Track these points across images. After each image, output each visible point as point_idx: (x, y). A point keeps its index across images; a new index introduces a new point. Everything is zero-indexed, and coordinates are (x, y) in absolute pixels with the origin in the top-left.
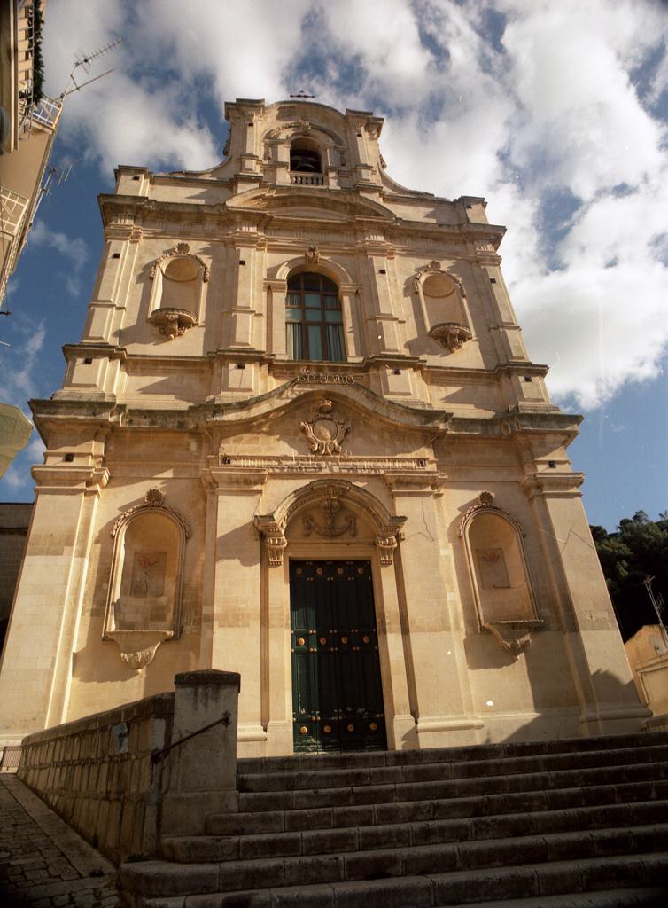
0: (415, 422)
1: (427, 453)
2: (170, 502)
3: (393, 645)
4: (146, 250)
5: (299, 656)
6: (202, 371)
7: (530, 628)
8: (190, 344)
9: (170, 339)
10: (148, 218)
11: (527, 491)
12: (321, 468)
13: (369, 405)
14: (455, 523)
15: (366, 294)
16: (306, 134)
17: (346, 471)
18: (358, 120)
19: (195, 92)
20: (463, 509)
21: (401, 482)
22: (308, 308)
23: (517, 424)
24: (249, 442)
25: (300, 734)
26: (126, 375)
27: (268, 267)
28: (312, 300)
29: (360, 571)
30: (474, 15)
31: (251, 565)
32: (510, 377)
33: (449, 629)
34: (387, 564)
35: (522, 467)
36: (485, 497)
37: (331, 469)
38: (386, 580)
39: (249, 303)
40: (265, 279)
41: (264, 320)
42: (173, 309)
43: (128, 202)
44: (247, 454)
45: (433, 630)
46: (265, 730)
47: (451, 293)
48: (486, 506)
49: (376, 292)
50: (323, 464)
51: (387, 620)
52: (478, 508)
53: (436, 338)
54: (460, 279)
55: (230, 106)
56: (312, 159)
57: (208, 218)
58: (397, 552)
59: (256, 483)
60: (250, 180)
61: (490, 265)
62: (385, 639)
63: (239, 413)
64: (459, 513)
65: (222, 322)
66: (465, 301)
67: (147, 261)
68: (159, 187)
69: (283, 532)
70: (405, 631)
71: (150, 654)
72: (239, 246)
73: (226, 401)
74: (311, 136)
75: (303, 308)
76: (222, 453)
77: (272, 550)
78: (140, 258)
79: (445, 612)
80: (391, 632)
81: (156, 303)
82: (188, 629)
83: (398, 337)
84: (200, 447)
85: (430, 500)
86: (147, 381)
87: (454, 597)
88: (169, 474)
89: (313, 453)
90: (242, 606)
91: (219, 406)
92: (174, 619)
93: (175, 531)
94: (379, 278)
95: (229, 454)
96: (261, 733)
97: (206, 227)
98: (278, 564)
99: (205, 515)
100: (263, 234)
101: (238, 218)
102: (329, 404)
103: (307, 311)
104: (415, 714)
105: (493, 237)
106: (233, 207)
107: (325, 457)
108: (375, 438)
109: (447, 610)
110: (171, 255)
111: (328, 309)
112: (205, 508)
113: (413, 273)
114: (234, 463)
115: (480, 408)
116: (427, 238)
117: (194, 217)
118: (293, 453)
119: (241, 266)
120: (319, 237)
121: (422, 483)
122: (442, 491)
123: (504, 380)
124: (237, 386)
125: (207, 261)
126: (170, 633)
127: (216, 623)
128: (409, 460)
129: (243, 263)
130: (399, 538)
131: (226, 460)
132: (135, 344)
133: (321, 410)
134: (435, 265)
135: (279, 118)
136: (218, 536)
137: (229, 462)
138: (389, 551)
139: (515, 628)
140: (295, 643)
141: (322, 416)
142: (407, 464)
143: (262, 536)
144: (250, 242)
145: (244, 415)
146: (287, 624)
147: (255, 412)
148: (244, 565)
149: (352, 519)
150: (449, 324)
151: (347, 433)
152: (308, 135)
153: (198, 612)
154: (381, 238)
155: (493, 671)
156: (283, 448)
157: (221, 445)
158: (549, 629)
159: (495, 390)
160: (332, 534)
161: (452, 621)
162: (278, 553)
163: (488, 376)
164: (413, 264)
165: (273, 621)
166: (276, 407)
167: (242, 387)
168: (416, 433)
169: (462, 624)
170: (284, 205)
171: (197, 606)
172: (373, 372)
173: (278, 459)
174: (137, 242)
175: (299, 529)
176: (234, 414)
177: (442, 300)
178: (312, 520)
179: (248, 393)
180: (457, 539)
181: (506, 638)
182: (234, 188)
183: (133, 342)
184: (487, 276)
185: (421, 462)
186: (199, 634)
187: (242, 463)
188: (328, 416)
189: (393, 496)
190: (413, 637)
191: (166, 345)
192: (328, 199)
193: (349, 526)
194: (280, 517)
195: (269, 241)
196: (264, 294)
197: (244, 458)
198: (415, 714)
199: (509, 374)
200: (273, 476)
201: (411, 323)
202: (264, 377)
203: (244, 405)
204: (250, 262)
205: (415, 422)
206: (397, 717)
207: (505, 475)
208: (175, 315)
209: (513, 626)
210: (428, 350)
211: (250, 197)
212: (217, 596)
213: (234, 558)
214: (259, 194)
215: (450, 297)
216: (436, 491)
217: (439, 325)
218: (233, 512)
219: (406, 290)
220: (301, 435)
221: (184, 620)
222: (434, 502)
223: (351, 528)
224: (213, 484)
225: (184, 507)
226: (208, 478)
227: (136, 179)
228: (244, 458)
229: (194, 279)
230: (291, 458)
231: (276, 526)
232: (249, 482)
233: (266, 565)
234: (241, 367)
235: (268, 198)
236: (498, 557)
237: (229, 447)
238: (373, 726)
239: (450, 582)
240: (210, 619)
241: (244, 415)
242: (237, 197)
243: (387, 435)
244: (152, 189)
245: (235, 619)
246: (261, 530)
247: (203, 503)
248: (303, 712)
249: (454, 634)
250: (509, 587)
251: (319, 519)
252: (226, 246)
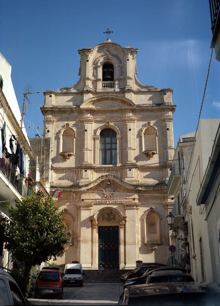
0: (132, 188)
1: (136, 196)
2: (69, 211)
3: (122, 248)
4: (57, 126)
5: (100, 250)
7: (157, 245)
8: (71, 163)
9: (66, 161)
10: (56, 113)
11: (164, 206)
12: (107, 202)
13: (120, 183)
14: (142, 216)
15: (125, 139)
16: (108, 59)
17: (113, 202)
18: (128, 51)
20: (145, 212)
21: (128, 206)
22: (107, 143)
23: (163, 187)
24: (88, 195)
25: (100, 266)
26: (55, 174)
27: (94, 129)
28: (108, 140)
29: (116, 229)
31: (89, 228)
32: (166, 169)
33: (136, 244)
34: (122, 228)
35: (165, 200)
36: (151, 208)
37: (109, 202)
38: (122, 232)
39: (88, 147)
40: (93, 136)
41: (93, 151)
42: (66, 152)
43: (50, 109)
44: (88, 198)
45: (132, 245)
46: (92, 266)
47: (154, 134)
48: (152, 210)
49: (127, 139)
50: (107, 201)
51: (121, 242)
52: (149, 212)
53: (145, 154)
54: (156, 128)
55: (80, 51)
57: (75, 111)
58: (125, 225)
59: (90, 207)
60: (88, 92)
61: (168, 122)
62: (120, 246)
63: (86, 188)
64: (144, 213)
65: (80, 157)
66: (157, 137)
67: (57, 131)
68: (58, 97)
69: (96, 220)
70: (125, 245)
71: (113, 124)
72: (85, 123)
74: (111, 60)
76: (82, 198)
77: (94, 225)
78: (55, 130)
79: (135, 240)
80: (122, 245)
81: (61, 151)
82: (75, 243)
83: (132, 155)
84: (76, 195)
85: (136, 211)
86: (61, 175)
87: (139, 237)
88: (68, 204)
89: (105, 197)
90: (87, 238)
91: (80, 186)
92: (72, 241)
93: (71, 218)
94: (129, 132)
95: (83, 199)
96: (91, 266)
97: (74, 115)
98: (95, 228)
99: (78, 214)
100: (92, 116)
101: (84, 111)
102: (109, 183)
103: (106, 144)
104: (125, 264)
105: (171, 109)
106: (82, 108)
107: (108, 199)
109: (136, 240)
110: (64, 128)
111: (113, 143)
112: (78, 213)
113: (141, 127)
114: (84, 201)
115: (155, 179)
116: (148, 111)
117: (70, 111)
118: (99, 197)
119: (85, 132)
120: (110, 115)
121: (133, 206)
122: (139, 208)
123: (164, 169)
124: (84, 178)
125: (75, 130)
126: (71, 244)
127: (81, 242)
128: (130, 199)
129: (86, 131)
130: (125, 221)
131: (83, 200)
132: (56, 163)
133: (108, 185)
134: (149, 123)
135: (98, 51)
136: (81, 221)
137: (83, 201)
138: (122, 225)
139: (153, 245)
140: (99, 245)
141: (108, 186)
142: (130, 200)
143: (92, 221)
144: (89, 121)
145: (87, 188)
146: (97, 242)
147: (90, 187)
148: (87, 228)
149: (114, 216)
150: (148, 151)
152: (109, 59)
153: (77, 239)
154: (131, 114)
155: (147, 255)
156: (97, 197)
157: (82, 196)
158: (163, 245)
159: (161, 172)
160: (109, 220)
161: (137, 242)
162: (95, 225)
163: (160, 168)
164: (142, 123)
165: (94, 242)
166: (95, 185)
167: (86, 178)
168: (133, 191)
169: (140, 243)
170: (99, 101)
171: (77, 238)
173: (95, 199)
174: (53, 124)
175: (101, 219)
176: (84, 188)
177: (151, 135)
178: (104, 216)
179: (88, 180)
180: (142, 220)
181: (150, 247)
182: (83, 95)
183: (55, 163)
184: (166, 127)
185: (134, 199)
186: (77, 244)
188: (109, 186)
189: (125, 209)
190: (127, 246)
191: (65, 163)
192: (114, 98)
193: (113, 218)
194: (95, 217)
195: (94, 119)
196: (93, 141)
197: (87, 199)
198: (125, 264)
199: (166, 168)
200: (94, 204)
201: (138, 149)
203: (86, 185)
204: (88, 130)
205: (132, 188)
206: (121, 264)
207: (159, 201)
208: (67, 154)
209: (152, 244)
210: (142, 159)
211: (88, 102)
212: (81, 236)
213: (84, 227)
214: (90, 101)
215: (153, 135)
216: (137, 208)
218: (85, 215)
219: (138, 135)
221: (74, 241)
222: (136, 211)
223: (114, 218)
224: (80, 207)
225: (73, 213)
226: (78, 206)
227: (51, 96)
228: (87, 199)
229: (72, 135)
230: (99, 199)
231: (94, 219)
232: (88, 207)
233: (93, 228)
235: (93, 100)
236: (154, 225)
237: (83, 197)
238: (117, 266)
239: (138, 232)
240: (80, 241)
241: (87, 188)
242: (83, 104)
244: (56, 98)
245: (86, 241)
246: (91, 219)
247: (77, 211)
248: (101, 262)
249: (137, 245)
250: (156, 233)
251: (106, 216)
252: (81, 122)
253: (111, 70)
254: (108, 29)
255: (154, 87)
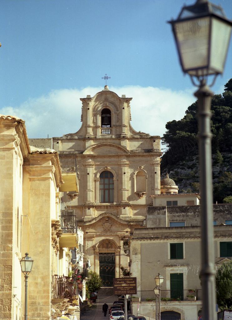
6: (80, 209)
13: (116, 219)
16: (107, 106)
19: (17, 135)
28: (107, 181)
30: (4, 129)
56: (121, 304)
59: (93, 238)
73: (98, 118)
75: (104, 184)
108: (118, 226)
119: (88, 175)
128: (124, 232)
140: (100, 269)
151: (112, 225)
165: (96, 265)
172: (119, 207)
187: (89, 234)
188: (108, 221)
196: (94, 183)
202: (94, 211)
203: (90, 221)
205: (126, 223)
217: (138, 192)
220: (102, 226)
234: (89, 209)
241: (90, 223)
243: (120, 226)
246: (94, 247)
251: (105, 245)
253: (108, 115)
254: (106, 74)
255: (145, 133)
